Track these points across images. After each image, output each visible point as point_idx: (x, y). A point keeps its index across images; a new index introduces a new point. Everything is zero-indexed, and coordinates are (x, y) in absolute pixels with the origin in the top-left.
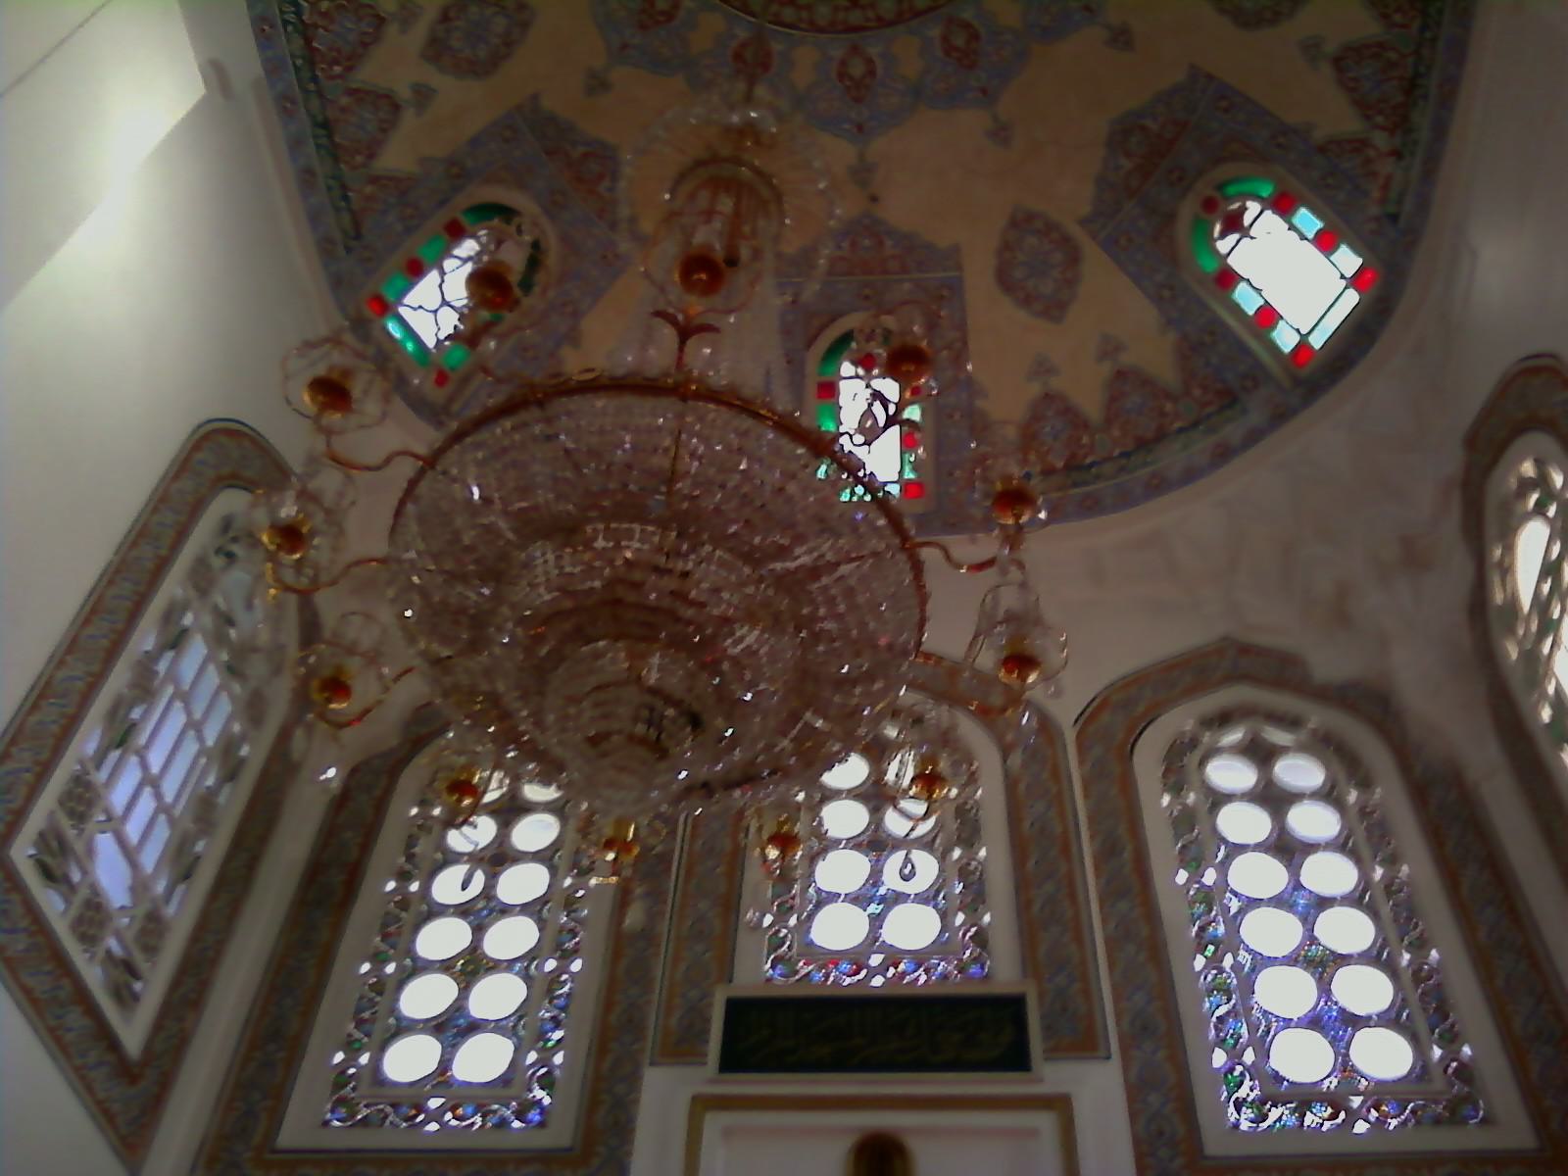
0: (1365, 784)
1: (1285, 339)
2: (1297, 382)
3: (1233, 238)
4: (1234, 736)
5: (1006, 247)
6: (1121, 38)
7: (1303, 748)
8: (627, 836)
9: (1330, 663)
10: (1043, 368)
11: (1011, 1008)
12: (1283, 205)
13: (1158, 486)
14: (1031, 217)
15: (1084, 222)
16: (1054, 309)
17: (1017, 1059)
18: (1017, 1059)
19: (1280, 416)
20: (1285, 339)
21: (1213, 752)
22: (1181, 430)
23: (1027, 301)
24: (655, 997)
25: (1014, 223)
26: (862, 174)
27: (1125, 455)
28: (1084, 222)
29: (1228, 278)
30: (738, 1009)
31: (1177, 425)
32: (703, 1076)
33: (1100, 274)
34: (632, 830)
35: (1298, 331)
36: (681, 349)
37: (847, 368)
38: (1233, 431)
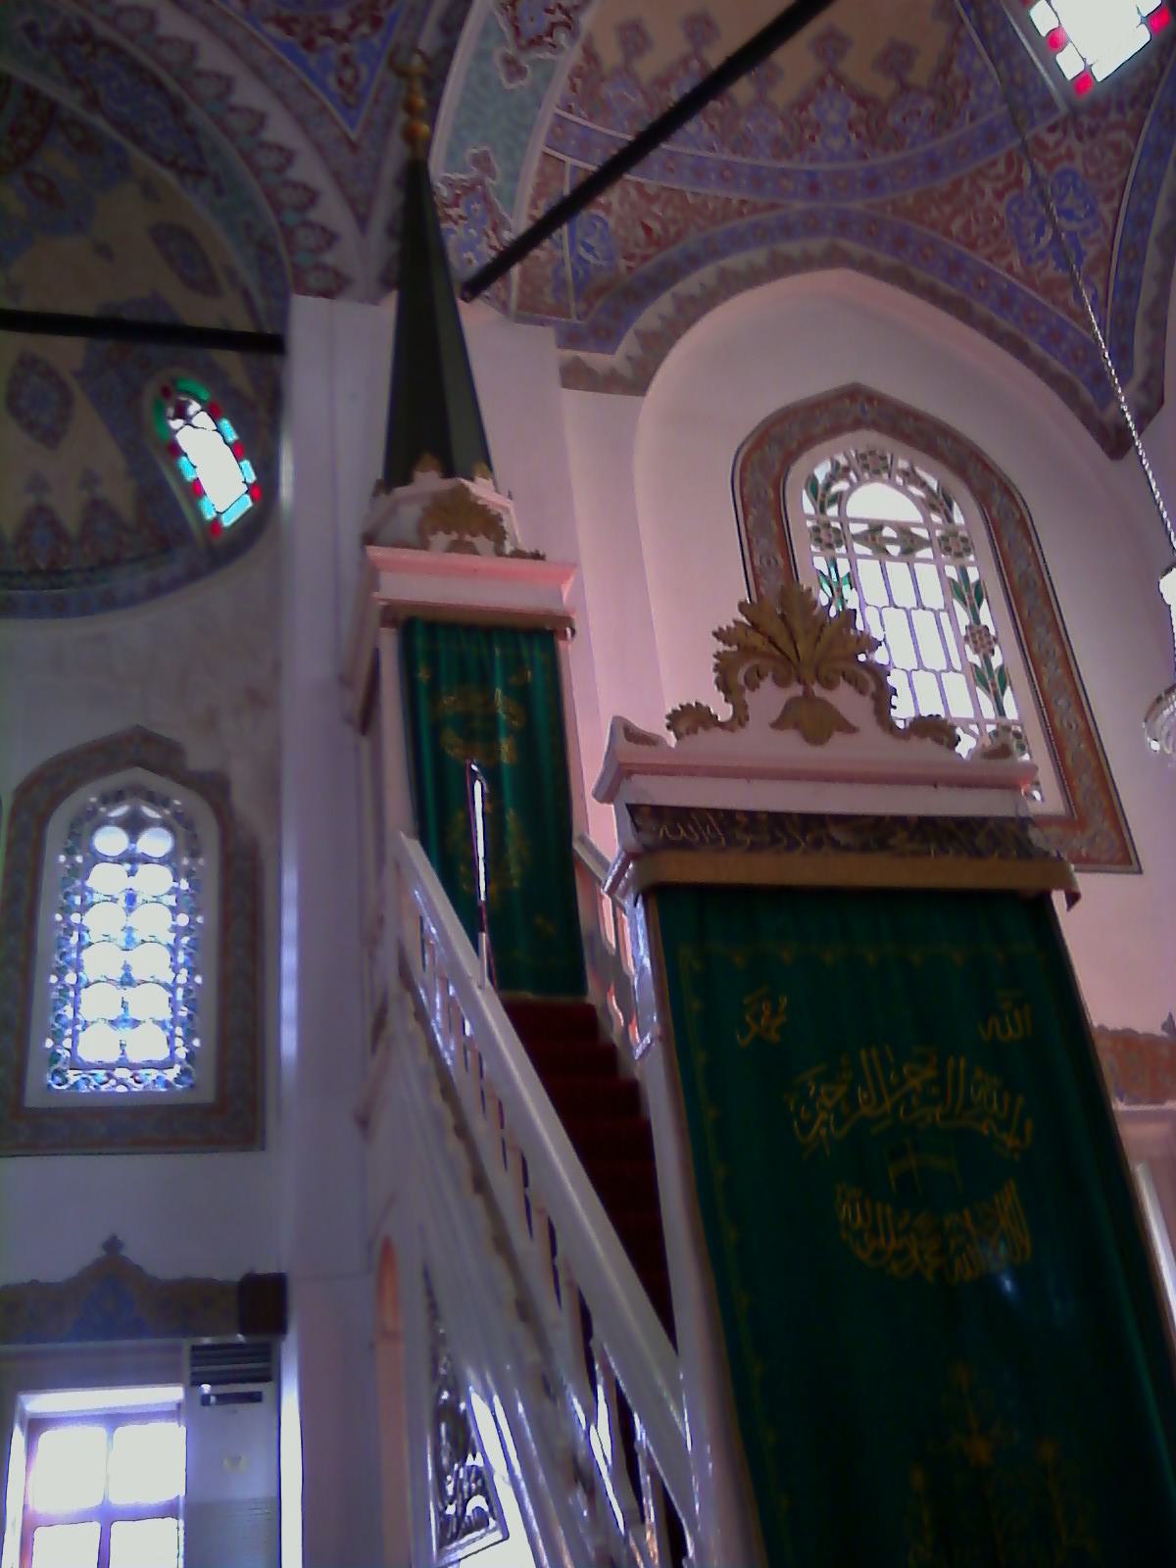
0: (194, 854)
1: (1069, 64)
4: (120, 811)
6: (104, 251)
7: (165, 824)
8: (620, 1532)
9: (199, 758)
10: (37, 484)
12: (214, 414)
16: (51, 437)
19: (193, 575)
20: (1069, 64)
21: (105, 822)
23: (30, 427)
27: (92, 570)
29: (175, 451)
33: (86, 419)
34: (614, 1003)
35: (1084, 59)
37: (176, 424)
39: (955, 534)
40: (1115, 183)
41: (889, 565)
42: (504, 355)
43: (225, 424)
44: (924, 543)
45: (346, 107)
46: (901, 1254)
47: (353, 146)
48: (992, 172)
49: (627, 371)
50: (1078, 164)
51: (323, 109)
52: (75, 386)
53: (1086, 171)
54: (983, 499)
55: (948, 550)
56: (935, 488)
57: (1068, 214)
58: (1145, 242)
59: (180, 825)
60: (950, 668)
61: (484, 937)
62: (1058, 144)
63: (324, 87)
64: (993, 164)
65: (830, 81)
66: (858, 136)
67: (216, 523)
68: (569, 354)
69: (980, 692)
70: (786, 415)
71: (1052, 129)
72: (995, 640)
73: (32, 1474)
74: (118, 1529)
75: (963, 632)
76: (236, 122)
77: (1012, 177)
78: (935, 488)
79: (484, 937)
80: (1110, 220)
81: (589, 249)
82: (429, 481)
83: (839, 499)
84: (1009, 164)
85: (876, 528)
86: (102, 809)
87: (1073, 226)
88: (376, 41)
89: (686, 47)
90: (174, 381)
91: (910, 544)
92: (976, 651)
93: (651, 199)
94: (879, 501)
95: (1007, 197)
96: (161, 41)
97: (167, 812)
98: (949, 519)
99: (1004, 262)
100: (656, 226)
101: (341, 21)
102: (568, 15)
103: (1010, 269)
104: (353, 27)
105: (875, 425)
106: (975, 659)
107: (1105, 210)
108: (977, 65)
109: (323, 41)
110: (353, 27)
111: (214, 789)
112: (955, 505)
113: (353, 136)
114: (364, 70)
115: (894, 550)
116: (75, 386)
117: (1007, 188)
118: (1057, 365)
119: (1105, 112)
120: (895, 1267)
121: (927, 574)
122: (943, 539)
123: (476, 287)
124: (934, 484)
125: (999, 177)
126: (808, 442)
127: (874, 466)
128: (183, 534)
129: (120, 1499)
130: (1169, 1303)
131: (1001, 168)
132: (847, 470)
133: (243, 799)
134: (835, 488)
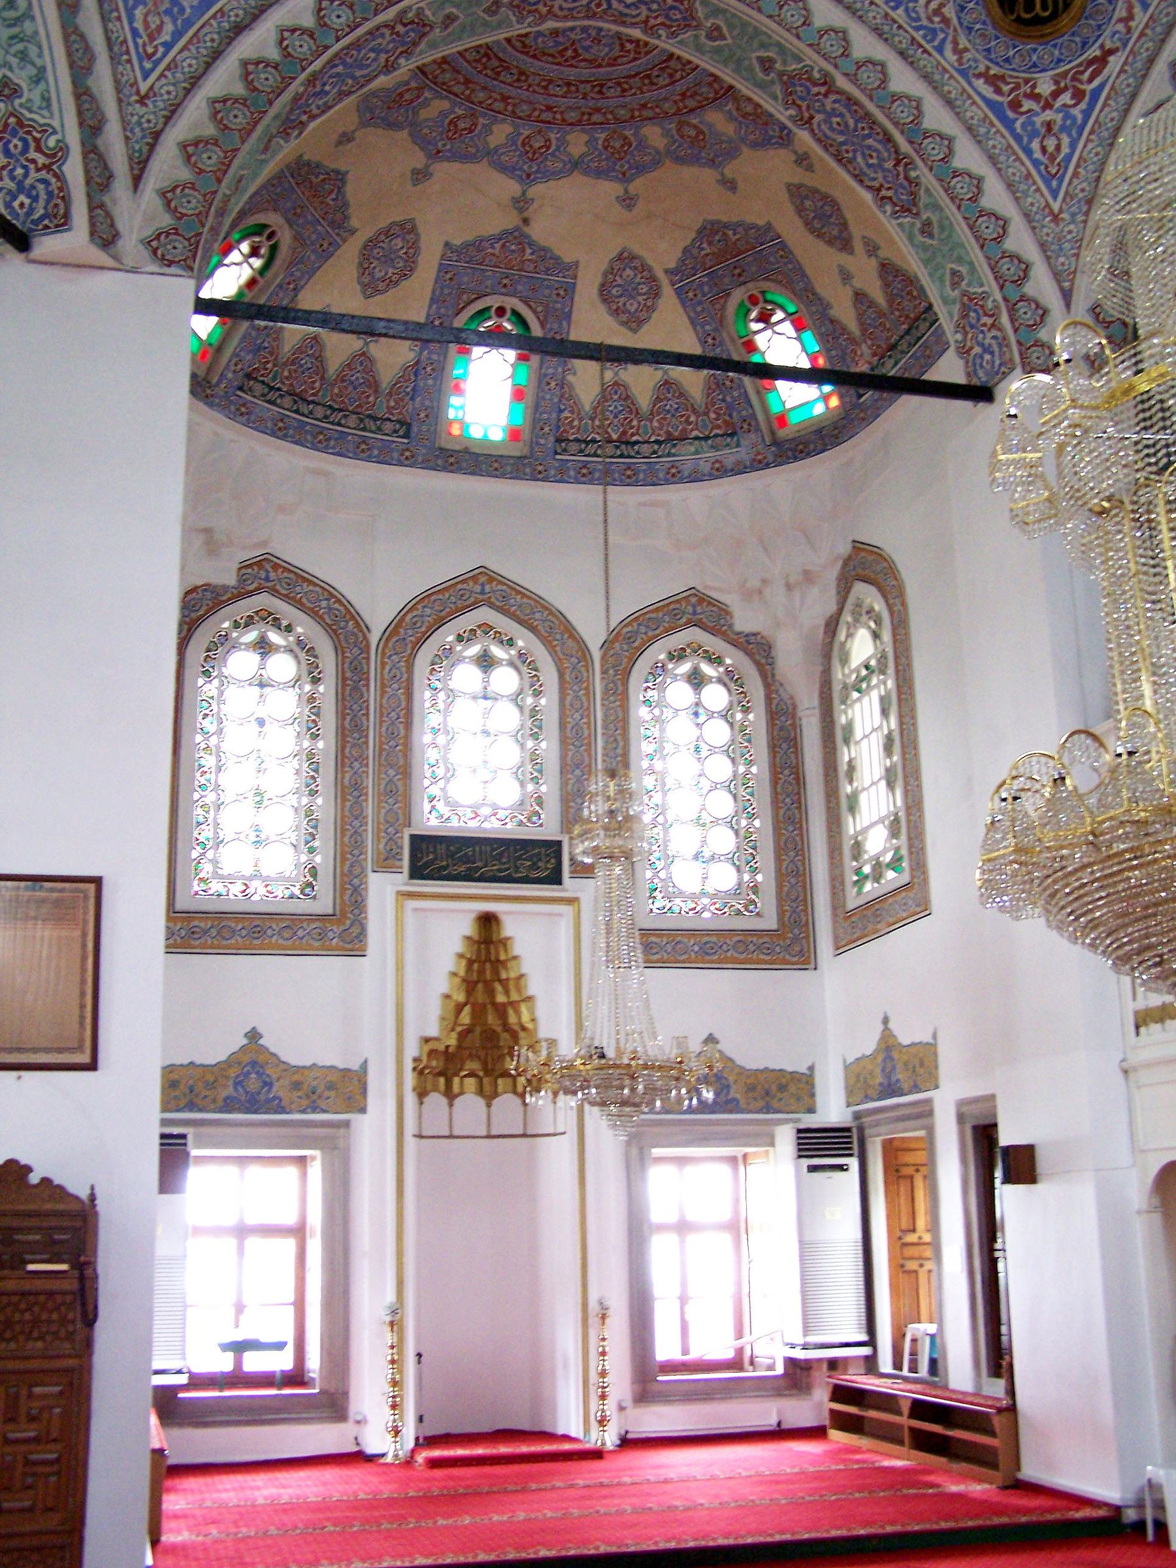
2: (776, 442)
3: (761, 326)
5: (610, 271)
9: (745, 620)
11: (554, 848)
12: (799, 326)
13: (674, 477)
14: (633, 257)
15: (667, 272)
17: (555, 878)
18: (555, 878)
19: (759, 464)
22: (696, 438)
23: (616, 312)
24: (370, 828)
25: (620, 257)
26: (521, 203)
28: (667, 272)
30: (416, 840)
31: (695, 433)
32: (399, 880)
36: (683, 1252)
37: (755, 326)
38: (730, 455)
43: (808, 336)
45: (1048, 178)
47: (1056, 218)
51: (1029, 175)
63: (1029, 152)
67: (782, 420)
73: (731, 1289)
74: (290, 1244)
86: (670, 666)
88: (1076, 112)
90: (763, 293)
96: (895, 97)
101: (1045, 87)
104: (1056, 94)
109: (1027, 105)
110: (1056, 94)
111: (758, 649)
113: (1056, 207)
114: (1065, 140)
128: (750, 422)
129: (251, 1221)
130: (978, 1197)
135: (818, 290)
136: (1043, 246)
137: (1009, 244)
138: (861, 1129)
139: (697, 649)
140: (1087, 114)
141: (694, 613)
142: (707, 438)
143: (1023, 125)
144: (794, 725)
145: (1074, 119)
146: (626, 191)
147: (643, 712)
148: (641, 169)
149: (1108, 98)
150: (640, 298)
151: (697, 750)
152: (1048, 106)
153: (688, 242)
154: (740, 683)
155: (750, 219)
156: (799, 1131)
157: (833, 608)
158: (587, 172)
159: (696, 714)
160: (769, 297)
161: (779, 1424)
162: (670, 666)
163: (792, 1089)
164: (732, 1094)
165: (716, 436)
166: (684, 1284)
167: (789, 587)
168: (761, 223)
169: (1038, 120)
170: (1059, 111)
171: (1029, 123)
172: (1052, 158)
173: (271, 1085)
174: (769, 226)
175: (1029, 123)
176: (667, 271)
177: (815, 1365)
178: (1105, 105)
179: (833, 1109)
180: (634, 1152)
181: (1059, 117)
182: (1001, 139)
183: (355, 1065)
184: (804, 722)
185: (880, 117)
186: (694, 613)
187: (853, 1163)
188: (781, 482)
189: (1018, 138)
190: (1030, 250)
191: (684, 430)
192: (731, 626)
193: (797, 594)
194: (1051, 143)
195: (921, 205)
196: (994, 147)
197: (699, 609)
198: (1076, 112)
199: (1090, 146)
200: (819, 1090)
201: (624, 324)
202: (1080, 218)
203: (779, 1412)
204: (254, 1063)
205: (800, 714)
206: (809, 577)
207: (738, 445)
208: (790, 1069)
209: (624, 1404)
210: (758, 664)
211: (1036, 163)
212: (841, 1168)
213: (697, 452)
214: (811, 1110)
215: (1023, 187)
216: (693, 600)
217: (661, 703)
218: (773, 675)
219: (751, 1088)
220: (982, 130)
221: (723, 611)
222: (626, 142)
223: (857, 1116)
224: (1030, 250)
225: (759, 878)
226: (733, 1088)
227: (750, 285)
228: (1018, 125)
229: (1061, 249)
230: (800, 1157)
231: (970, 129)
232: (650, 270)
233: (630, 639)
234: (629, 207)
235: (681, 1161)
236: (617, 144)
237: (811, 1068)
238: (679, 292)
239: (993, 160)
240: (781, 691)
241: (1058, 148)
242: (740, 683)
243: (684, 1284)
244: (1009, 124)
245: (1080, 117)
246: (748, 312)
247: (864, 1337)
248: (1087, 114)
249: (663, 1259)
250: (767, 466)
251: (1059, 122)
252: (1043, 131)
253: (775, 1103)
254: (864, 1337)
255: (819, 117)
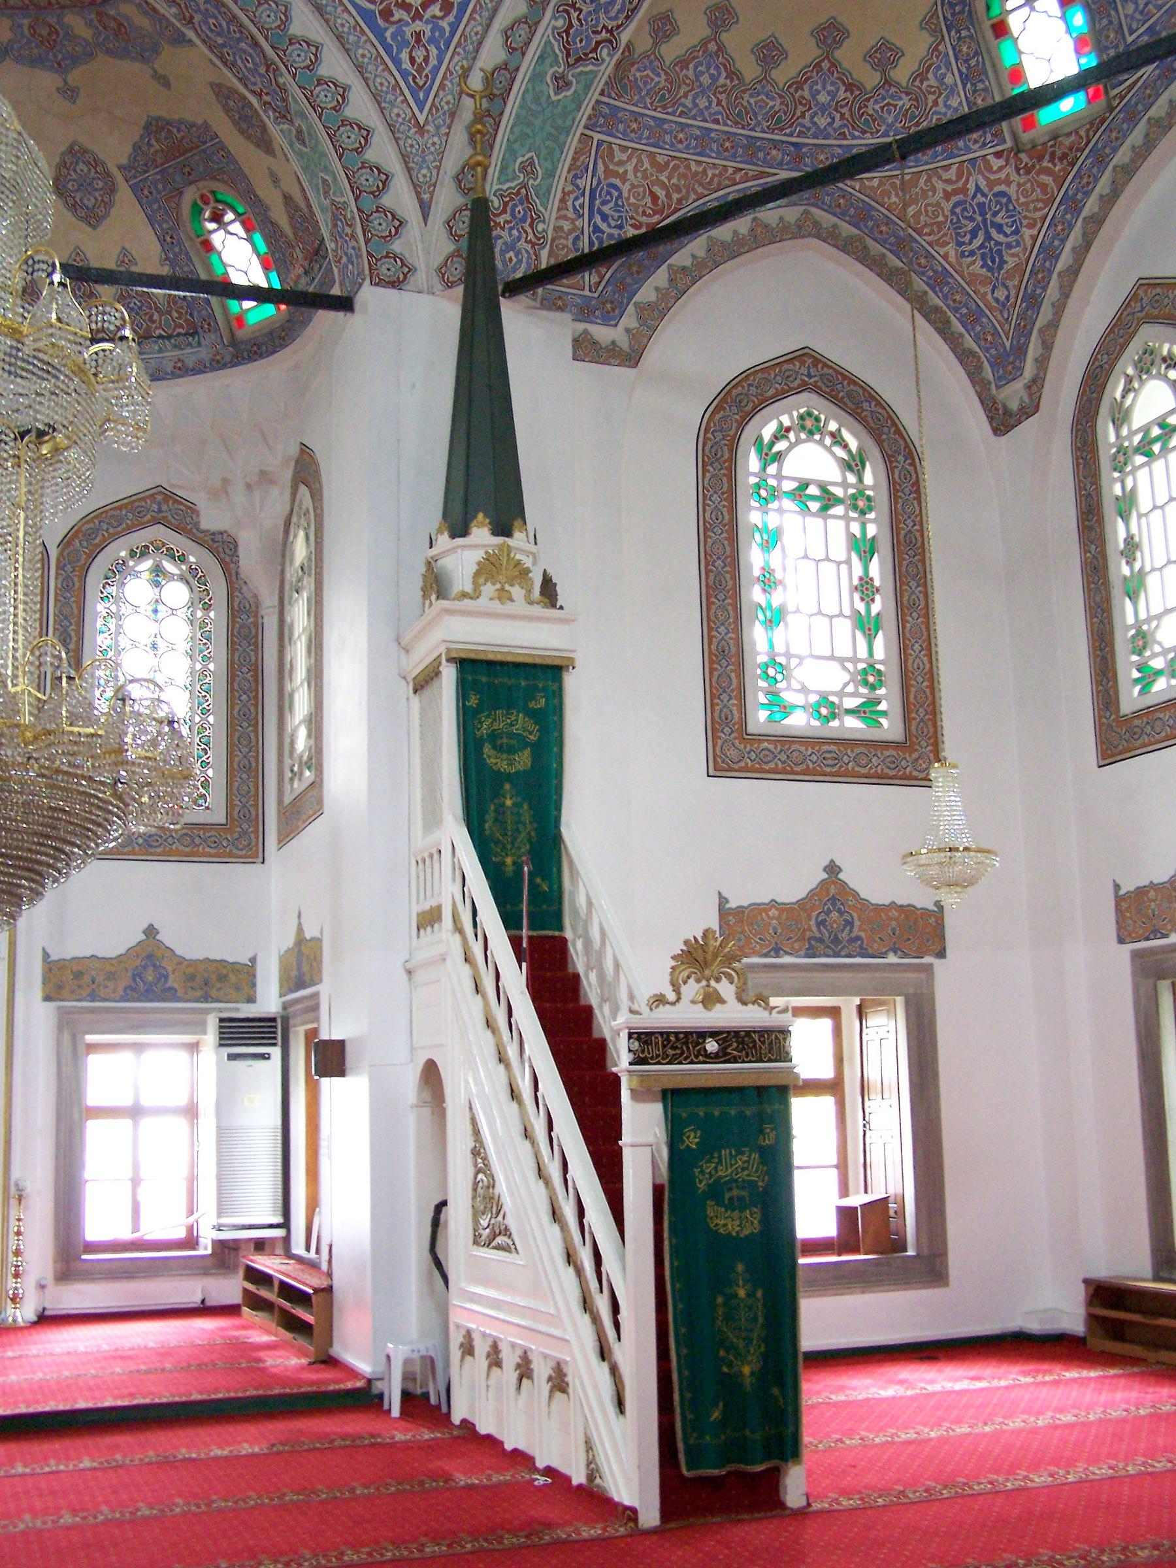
0: (207, 608)
2: (234, 342)
7: (182, 578)
9: (211, 519)
12: (248, 228)
15: (120, 168)
19: (217, 364)
22: (160, 337)
25: (70, 150)
29: (208, 246)
37: (212, 226)
38: (191, 355)
39: (861, 492)
40: (1038, 214)
41: (809, 519)
42: (533, 339)
43: (258, 237)
44: (840, 501)
46: (725, 1225)
47: (421, 130)
48: (945, 176)
49: (624, 342)
50: (1012, 191)
52: (119, 177)
53: (1018, 199)
54: (889, 460)
55: (855, 507)
56: (854, 450)
57: (999, 228)
58: (1051, 272)
59: (194, 578)
60: (841, 614)
61: (524, 965)
62: (1000, 169)
63: (397, 62)
64: (947, 168)
65: (825, 65)
66: (842, 116)
68: (582, 326)
69: (859, 634)
70: (746, 376)
71: (998, 155)
72: (878, 590)
73: (184, 1172)
75: (856, 582)
76: (325, 97)
77: (960, 184)
78: (854, 450)
79: (524, 965)
80: (1029, 243)
81: (605, 218)
82: (481, 535)
83: (779, 457)
84: (959, 175)
85: (804, 484)
86: (131, 563)
87: (1000, 238)
89: (707, 32)
91: (828, 500)
92: (862, 599)
93: (660, 168)
94: (813, 461)
95: (955, 199)
97: (184, 567)
98: (861, 480)
99: (942, 251)
100: (661, 193)
102: (612, 34)
103: (945, 257)
105: (816, 390)
106: (860, 606)
107: (1027, 233)
108: (949, 80)
109: (399, 14)
111: (223, 547)
112: (868, 465)
114: (434, 51)
115: (814, 506)
116: (119, 177)
117: (955, 192)
118: (969, 342)
119: (1040, 158)
120: (721, 1231)
121: (837, 529)
122: (854, 497)
123: (514, 288)
124: (853, 444)
125: (949, 181)
126: (763, 403)
127: (809, 426)
131: (952, 174)
132: (788, 430)
133: (250, 561)
134: (776, 448)
135: (259, 193)
136: (405, 158)
137: (370, 155)
138: (286, 1020)
139: (158, 546)
140: (454, 28)
141: (160, 511)
142: (169, 337)
143: (394, 36)
144: (256, 625)
145: (442, 30)
146: (66, 82)
147: (101, 607)
148: (75, 61)
149: (474, 11)
150: (97, 194)
151: (154, 646)
152: (418, 16)
153: (137, 138)
154: (202, 581)
155: (190, 117)
156: (222, 1020)
157: (288, 507)
158: (19, 60)
159: (156, 611)
160: (220, 197)
161: (203, 1301)
162: (131, 563)
163: (233, 978)
164: (170, 983)
165: (179, 335)
166: (136, 1166)
167: (249, 487)
168: (200, 122)
169: (408, 31)
170: (427, 22)
171: (399, 33)
172: (420, 70)
173: (166, 977)
174: (206, 127)
175: (399, 33)
176: (120, 167)
177: (243, 1246)
178: (471, 18)
179: (269, 1000)
180: (67, 1037)
181: (428, 29)
182: (366, 51)
183: (244, 959)
184: (266, 620)
185: (246, 22)
186: (160, 511)
187: (276, 1052)
188: (240, 382)
189: (388, 49)
190: (393, 163)
191: (148, 329)
192: (196, 525)
193: (257, 495)
194: (419, 55)
195: (293, 112)
196: (363, 56)
197: (164, 507)
198: (444, 24)
199: (456, 58)
200: (259, 980)
201: (81, 219)
202: (444, 130)
203: (203, 1291)
204: (150, 957)
205: (262, 612)
206: (266, 477)
207: (199, 344)
208: (231, 960)
209: (43, 1282)
210: (221, 562)
211: (404, 74)
212: (265, 1057)
213: (160, 351)
214: (251, 1000)
215: (390, 97)
216: (159, 498)
217: (118, 600)
218: (237, 573)
219: (192, 978)
220: (352, 38)
221: (191, 509)
222: (53, 31)
223: (285, 1006)
224: (393, 163)
225: (210, 772)
226: (171, 977)
227: (201, 184)
228: (388, 34)
229: (424, 161)
230: (221, 1045)
231: (339, 37)
232: (103, 164)
233: (90, 535)
234: (72, 99)
235: (138, 1047)
236: (45, 33)
237: (253, 960)
238: (136, 190)
239: (360, 69)
240: (245, 589)
241: (426, 59)
242: (202, 581)
243: (136, 1166)
244: (379, 34)
245: (448, 29)
246: (201, 212)
247: (278, 1219)
248: (454, 28)
249: (101, 1142)
250: (225, 366)
251: (428, 34)
252: (413, 41)
253: (214, 993)
254: (278, 1219)
255: (604, 21)
